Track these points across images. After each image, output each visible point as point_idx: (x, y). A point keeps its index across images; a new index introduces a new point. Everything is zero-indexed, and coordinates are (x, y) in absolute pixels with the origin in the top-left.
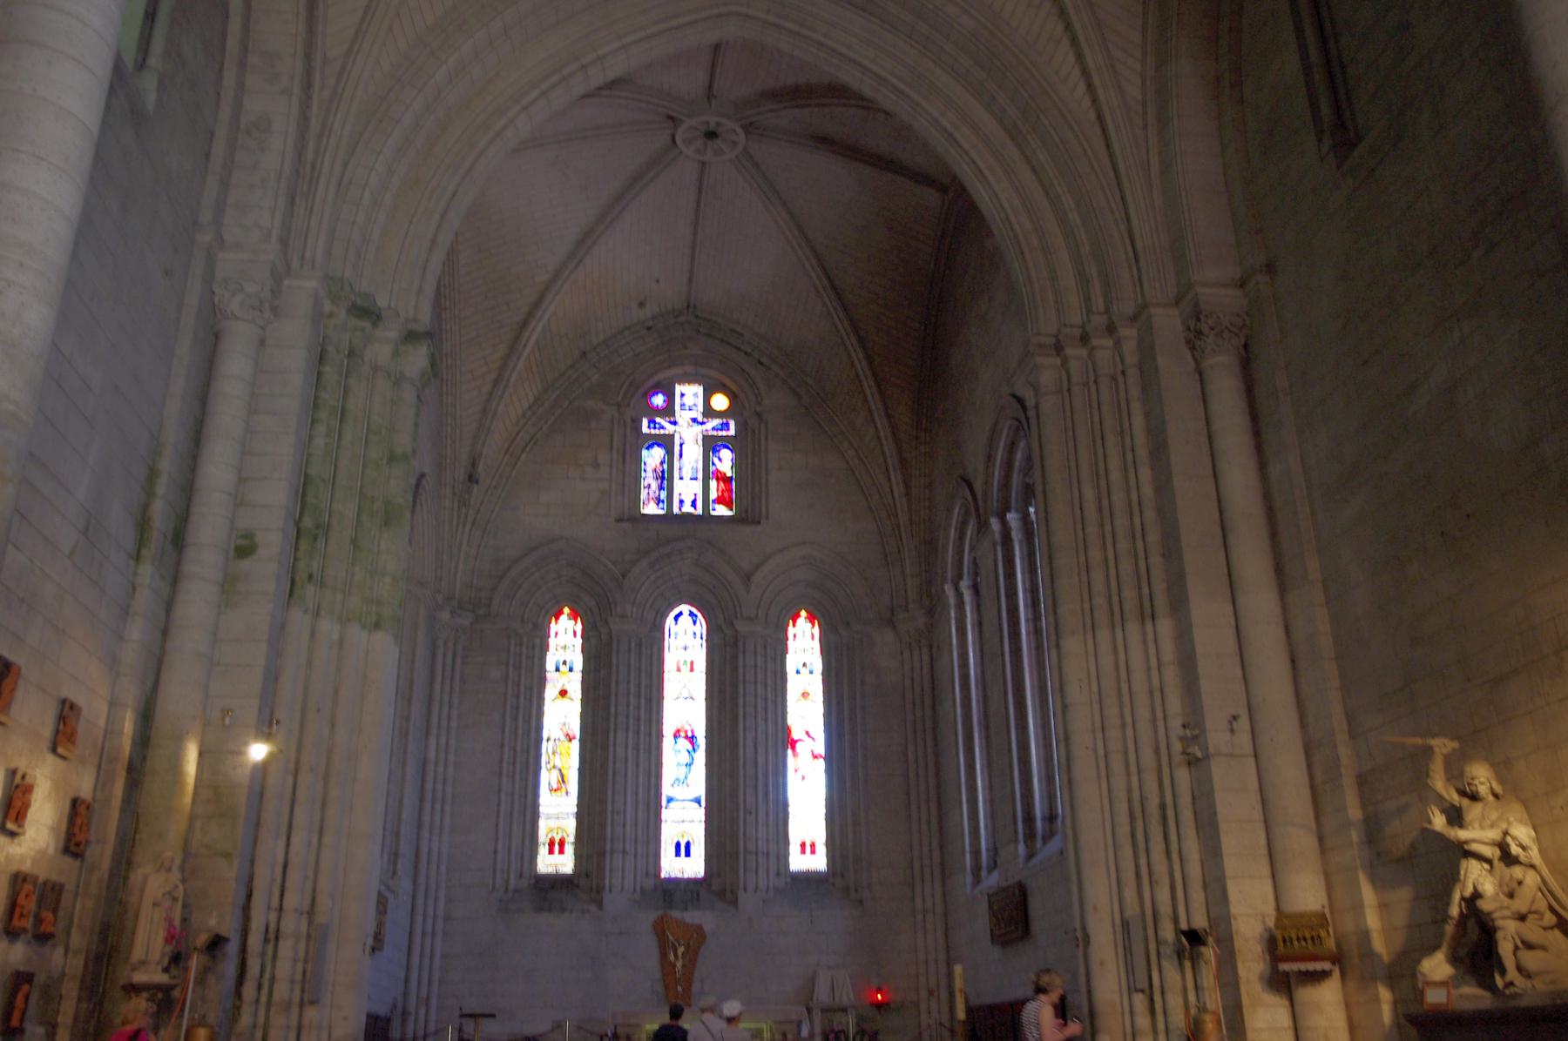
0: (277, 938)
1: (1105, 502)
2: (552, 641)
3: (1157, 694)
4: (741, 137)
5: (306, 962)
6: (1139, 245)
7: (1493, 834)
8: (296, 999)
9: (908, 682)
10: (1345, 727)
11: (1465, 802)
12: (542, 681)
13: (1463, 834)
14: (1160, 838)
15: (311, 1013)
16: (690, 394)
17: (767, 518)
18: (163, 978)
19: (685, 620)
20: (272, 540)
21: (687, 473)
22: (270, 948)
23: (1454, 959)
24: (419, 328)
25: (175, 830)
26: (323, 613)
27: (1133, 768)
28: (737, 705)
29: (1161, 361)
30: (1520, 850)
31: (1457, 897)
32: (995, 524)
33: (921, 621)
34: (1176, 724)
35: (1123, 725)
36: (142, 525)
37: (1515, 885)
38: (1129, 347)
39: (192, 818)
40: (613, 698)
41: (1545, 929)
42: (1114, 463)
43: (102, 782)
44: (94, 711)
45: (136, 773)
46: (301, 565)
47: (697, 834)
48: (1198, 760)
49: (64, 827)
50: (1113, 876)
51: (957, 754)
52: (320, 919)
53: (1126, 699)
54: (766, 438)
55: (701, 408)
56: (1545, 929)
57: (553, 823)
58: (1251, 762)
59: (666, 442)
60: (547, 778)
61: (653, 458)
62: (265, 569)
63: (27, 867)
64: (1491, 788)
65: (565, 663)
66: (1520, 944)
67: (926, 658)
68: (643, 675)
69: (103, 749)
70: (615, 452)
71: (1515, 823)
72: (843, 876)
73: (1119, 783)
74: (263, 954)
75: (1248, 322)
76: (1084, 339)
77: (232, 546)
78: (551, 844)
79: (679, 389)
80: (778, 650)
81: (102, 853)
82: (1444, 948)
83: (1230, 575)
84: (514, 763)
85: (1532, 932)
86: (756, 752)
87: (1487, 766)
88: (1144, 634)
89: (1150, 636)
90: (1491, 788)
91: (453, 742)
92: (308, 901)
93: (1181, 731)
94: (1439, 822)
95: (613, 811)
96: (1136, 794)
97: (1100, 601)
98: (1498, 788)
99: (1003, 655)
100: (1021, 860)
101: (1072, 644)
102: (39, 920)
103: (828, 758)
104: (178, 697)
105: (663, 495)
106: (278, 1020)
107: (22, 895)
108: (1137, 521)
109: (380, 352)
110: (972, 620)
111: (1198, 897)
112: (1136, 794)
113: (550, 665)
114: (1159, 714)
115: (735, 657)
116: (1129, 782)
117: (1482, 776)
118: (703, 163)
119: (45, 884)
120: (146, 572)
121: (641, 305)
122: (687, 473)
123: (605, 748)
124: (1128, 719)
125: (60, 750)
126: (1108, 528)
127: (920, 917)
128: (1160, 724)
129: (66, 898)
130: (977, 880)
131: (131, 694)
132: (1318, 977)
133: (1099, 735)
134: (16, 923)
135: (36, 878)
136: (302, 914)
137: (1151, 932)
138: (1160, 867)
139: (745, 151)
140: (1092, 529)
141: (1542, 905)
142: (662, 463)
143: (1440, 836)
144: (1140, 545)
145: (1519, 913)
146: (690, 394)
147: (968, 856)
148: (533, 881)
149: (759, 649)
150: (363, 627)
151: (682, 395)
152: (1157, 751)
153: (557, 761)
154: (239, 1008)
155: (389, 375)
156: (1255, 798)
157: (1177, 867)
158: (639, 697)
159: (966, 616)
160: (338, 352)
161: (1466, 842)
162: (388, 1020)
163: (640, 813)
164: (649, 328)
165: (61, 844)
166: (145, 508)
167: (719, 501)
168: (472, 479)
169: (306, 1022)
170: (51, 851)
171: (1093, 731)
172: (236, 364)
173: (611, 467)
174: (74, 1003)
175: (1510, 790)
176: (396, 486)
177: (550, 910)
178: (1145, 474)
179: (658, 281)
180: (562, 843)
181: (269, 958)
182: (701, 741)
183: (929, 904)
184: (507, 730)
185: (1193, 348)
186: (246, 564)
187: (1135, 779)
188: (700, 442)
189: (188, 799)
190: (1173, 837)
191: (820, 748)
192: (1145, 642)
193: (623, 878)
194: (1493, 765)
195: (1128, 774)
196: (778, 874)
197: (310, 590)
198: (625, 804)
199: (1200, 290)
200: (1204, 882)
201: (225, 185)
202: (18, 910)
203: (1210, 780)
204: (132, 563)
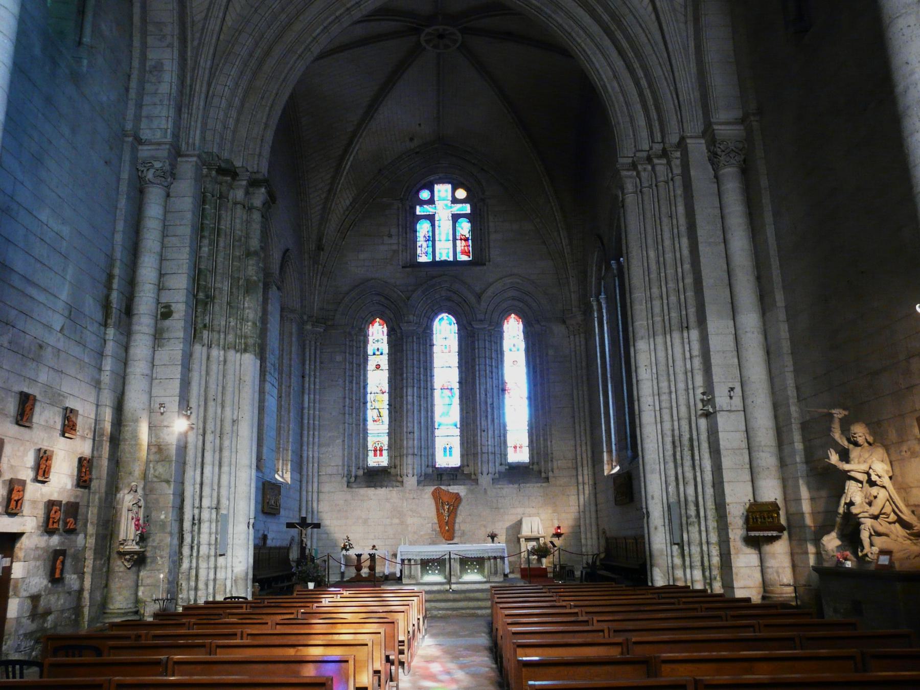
0: (200, 523)
1: (661, 259)
2: (370, 339)
3: (689, 374)
5: (216, 533)
6: (681, 99)
7: (864, 467)
8: (212, 553)
9: (573, 354)
10: (795, 394)
11: (851, 446)
13: (846, 467)
14: (689, 458)
15: (221, 560)
17: (489, 261)
18: (137, 548)
19: (445, 322)
20: (180, 309)
21: (443, 237)
22: (196, 527)
23: (841, 537)
24: (260, 176)
25: (137, 469)
26: (213, 346)
27: (675, 418)
29: (692, 173)
30: (877, 477)
31: (843, 502)
33: (579, 318)
34: (700, 391)
35: (670, 393)
36: (106, 306)
37: (872, 498)
38: (676, 163)
39: (148, 462)
40: (405, 369)
41: (890, 523)
42: (667, 235)
43: (96, 445)
44: (86, 412)
45: (115, 440)
46: (199, 320)
47: (456, 443)
48: (711, 413)
49: (75, 473)
50: (663, 478)
52: (223, 511)
53: (672, 378)
56: (890, 523)
58: (743, 413)
59: (431, 218)
60: (371, 414)
61: (423, 228)
62: (177, 325)
63: (55, 497)
64: (866, 439)
65: (378, 350)
66: (767, 595)
68: (422, 355)
69: (95, 429)
70: (400, 227)
71: (876, 462)
72: (537, 463)
73: (667, 426)
74: (192, 531)
75: (746, 146)
76: (649, 159)
77: (159, 312)
78: (375, 450)
79: (437, 187)
80: (497, 337)
81: (99, 484)
82: (836, 531)
83: (732, 303)
85: (881, 526)
87: (864, 425)
88: (683, 338)
90: (866, 439)
91: (317, 397)
93: (701, 396)
94: (834, 458)
96: (677, 432)
97: (658, 319)
98: (870, 439)
101: (642, 345)
102: (66, 523)
104: (135, 400)
105: (430, 250)
106: (203, 565)
107: (53, 512)
108: (679, 270)
109: (239, 194)
112: (677, 432)
113: (370, 352)
114: (690, 386)
116: (673, 425)
117: (860, 432)
120: (111, 332)
121: (411, 139)
122: (443, 237)
124: (673, 389)
126: (663, 274)
128: (691, 392)
129: (82, 510)
131: (107, 398)
132: (772, 540)
133: (656, 397)
134: (50, 526)
135: (61, 502)
136: (212, 509)
137: (683, 512)
138: (689, 475)
140: (654, 276)
141: (888, 509)
143: (834, 466)
144: (681, 285)
145: (872, 515)
146: (443, 191)
150: (237, 351)
152: (689, 407)
153: (377, 405)
154: (182, 559)
155: (244, 207)
157: (698, 474)
160: (213, 196)
161: (849, 471)
164: (417, 153)
165: (75, 482)
166: (107, 297)
167: (463, 252)
168: (320, 248)
169: (219, 565)
170: (69, 486)
171: (654, 396)
172: (154, 210)
173: (399, 235)
174: (92, 562)
175: (879, 439)
176: (252, 270)
178: (685, 242)
179: (420, 125)
180: (381, 450)
185: (712, 164)
186: (167, 323)
187: (676, 423)
188: (451, 218)
189: (144, 453)
190: (697, 457)
192: (683, 343)
194: (868, 425)
195: (673, 421)
196: (501, 464)
197: (205, 333)
199: (716, 127)
200: (714, 483)
201: (139, 105)
203: (716, 424)
204: (102, 328)
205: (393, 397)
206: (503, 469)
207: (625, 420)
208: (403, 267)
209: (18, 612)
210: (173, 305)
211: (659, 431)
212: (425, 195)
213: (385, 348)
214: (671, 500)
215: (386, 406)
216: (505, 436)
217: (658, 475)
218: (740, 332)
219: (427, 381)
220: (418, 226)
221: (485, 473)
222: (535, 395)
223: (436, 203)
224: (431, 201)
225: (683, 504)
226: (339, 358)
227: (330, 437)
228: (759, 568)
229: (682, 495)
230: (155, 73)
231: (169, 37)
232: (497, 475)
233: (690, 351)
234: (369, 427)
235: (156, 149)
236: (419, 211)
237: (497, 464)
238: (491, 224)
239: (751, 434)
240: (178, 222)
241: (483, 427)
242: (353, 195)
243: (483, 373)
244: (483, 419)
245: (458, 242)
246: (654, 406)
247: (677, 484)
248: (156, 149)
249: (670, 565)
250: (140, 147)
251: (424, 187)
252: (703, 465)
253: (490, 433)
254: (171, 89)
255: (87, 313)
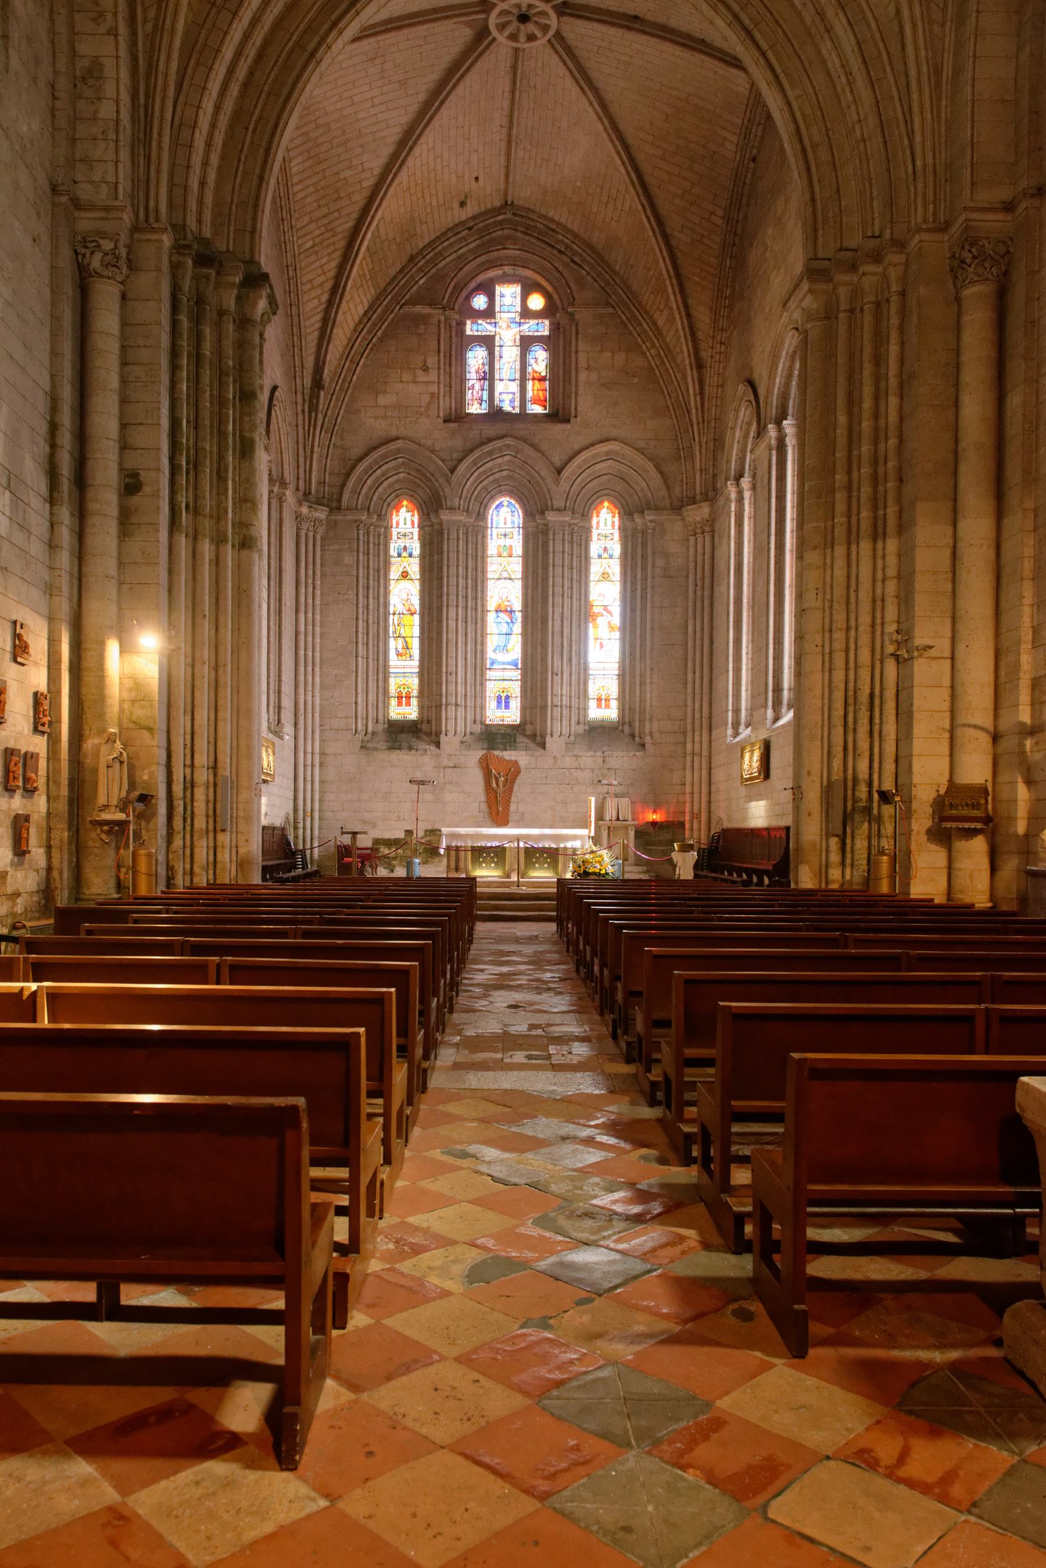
0: (193, 787)
2: (394, 532)
4: (553, 21)
9: (691, 565)
12: (387, 564)
14: (866, 721)
16: (508, 294)
19: (505, 511)
21: (505, 374)
27: (852, 665)
28: (547, 587)
32: (772, 431)
35: (848, 629)
36: (52, 473)
51: (728, 629)
53: (853, 606)
54: (577, 339)
55: (519, 309)
57: (401, 681)
58: (949, 661)
59: (488, 342)
61: (476, 358)
65: (405, 548)
67: (708, 545)
72: (630, 725)
73: (839, 675)
79: (499, 289)
80: (581, 538)
84: (367, 634)
86: (562, 626)
88: (874, 550)
89: (880, 553)
91: (318, 617)
92: (212, 759)
95: (447, 673)
99: (769, 550)
100: (769, 722)
103: (623, 629)
105: (485, 397)
107: (12, 764)
110: (750, 513)
111: (889, 767)
113: (393, 552)
115: (545, 544)
116: (846, 675)
118: (516, 50)
119: (26, 753)
121: (462, 204)
123: (440, 621)
124: (853, 623)
125: (19, 659)
127: (689, 759)
128: (878, 628)
130: (736, 734)
132: (972, 833)
133: (827, 635)
134: (12, 783)
137: (850, 793)
138: (863, 744)
139: (558, 35)
142: (483, 364)
146: (508, 294)
147: (730, 714)
148: (386, 726)
149: (566, 537)
151: (502, 296)
156: (946, 694)
157: (876, 744)
158: (467, 578)
159: (744, 510)
162: (283, 829)
163: (469, 674)
167: (535, 401)
173: (439, 369)
177: (400, 748)
179: (477, 179)
180: (408, 697)
181: (188, 800)
182: (519, 616)
183: (697, 750)
184: (360, 606)
186: (135, 500)
190: (877, 721)
191: (616, 620)
193: (456, 725)
195: (847, 669)
198: (456, 666)
202: (11, 774)
203: (912, 676)
205: (426, 620)
206: (581, 729)
207: (767, 666)
208: (445, 421)
209: (38, 884)
210: (142, 473)
211: (827, 683)
212: (480, 302)
213: (416, 548)
214: (834, 778)
215: (416, 631)
216: (586, 683)
217: (819, 742)
218: (961, 545)
219: (476, 599)
220: (470, 355)
221: (556, 734)
222: (633, 625)
223: (498, 315)
224: (489, 313)
225: (850, 783)
226: (348, 559)
227: (336, 676)
228: (945, 871)
229: (850, 772)
230: (91, 82)
231: (109, 16)
232: (572, 738)
233: (883, 569)
234: (391, 663)
235: (103, 219)
236: (471, 329)
237: (573, 722)
238: (582, 356)
239: (959, 690)
240: (141, 342)
241: (555, 670)
242: (369, 297)
243: (558, 589)
244: (557, 656)
245: (530, 385)
246: (823, 646)
247: (845, 757)
248: (103, 219)
249: (824, 863)
250: (77, 214)
251: (480, 289)
252: (884, 733)
253: (566, 676)
254: (118, 112)
255: (29, 482)
